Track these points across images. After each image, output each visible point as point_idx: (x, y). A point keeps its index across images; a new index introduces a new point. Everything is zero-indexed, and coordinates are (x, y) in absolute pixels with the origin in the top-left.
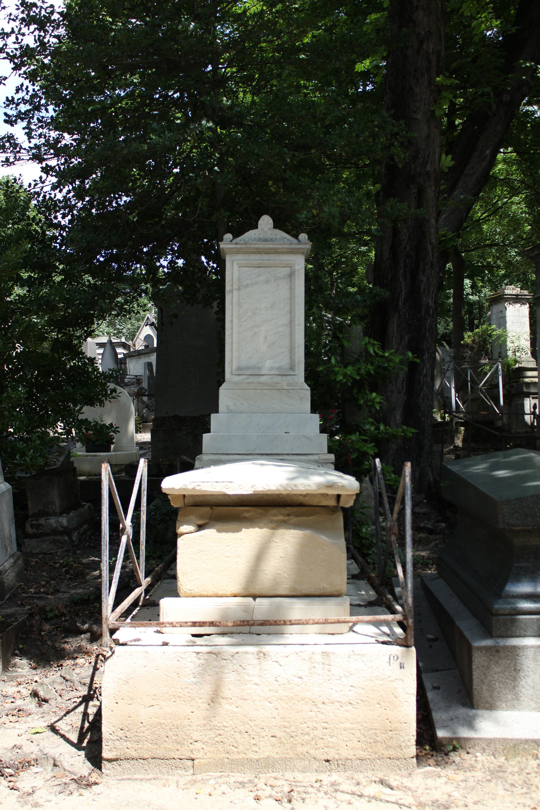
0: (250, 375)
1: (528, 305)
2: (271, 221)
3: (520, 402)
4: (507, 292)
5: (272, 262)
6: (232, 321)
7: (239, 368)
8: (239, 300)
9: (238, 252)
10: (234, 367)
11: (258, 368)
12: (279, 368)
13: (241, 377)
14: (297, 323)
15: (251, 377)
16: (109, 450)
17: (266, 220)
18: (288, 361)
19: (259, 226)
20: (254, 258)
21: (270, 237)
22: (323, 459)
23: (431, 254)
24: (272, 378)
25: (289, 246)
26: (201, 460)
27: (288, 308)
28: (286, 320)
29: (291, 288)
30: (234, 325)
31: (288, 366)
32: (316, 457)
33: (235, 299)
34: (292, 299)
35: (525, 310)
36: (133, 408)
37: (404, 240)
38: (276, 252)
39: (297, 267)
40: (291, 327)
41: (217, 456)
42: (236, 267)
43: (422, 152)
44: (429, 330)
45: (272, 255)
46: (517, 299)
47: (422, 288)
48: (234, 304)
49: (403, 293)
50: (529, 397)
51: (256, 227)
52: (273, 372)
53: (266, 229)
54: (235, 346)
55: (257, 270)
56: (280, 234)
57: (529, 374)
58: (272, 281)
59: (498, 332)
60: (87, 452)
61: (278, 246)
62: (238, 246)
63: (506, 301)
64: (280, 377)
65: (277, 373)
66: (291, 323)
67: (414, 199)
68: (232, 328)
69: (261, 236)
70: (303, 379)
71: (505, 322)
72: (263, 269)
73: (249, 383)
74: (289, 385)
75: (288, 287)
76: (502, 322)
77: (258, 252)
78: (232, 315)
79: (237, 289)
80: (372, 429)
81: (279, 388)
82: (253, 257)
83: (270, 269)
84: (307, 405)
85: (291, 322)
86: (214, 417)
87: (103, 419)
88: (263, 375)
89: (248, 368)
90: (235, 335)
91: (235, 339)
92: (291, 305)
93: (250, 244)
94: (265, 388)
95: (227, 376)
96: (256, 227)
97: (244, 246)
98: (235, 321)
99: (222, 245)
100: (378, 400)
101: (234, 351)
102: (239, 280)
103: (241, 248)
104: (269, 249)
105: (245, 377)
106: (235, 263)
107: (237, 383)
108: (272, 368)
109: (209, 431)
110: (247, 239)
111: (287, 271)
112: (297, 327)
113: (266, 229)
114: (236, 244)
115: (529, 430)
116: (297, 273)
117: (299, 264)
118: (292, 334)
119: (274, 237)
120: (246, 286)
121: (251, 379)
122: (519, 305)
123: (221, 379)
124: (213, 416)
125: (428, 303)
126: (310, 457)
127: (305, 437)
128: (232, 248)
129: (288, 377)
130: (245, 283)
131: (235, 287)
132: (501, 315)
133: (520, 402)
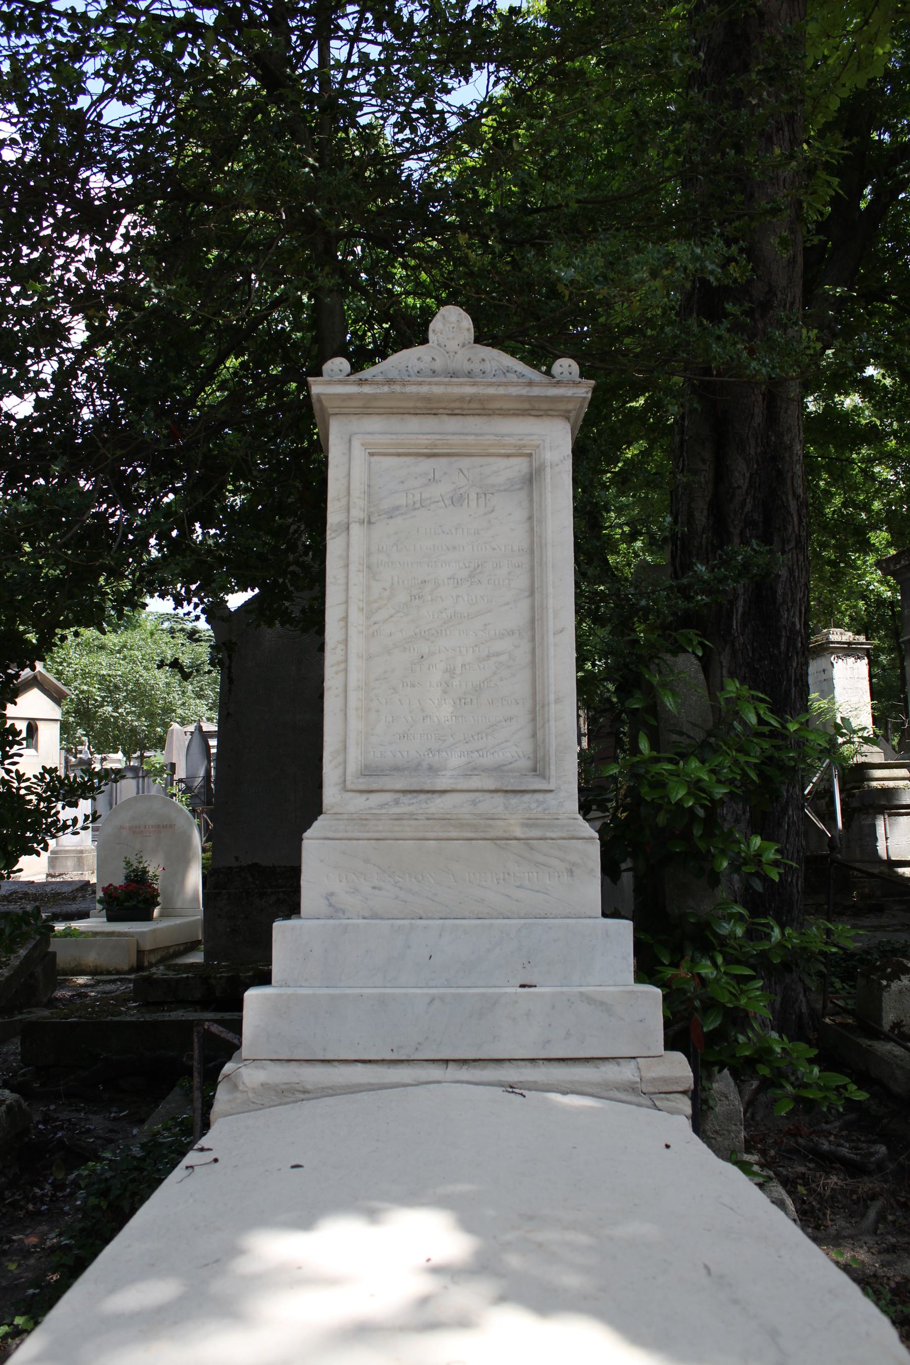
0: (404, 792)
1: (866, 661)
2: (467, 322)
3: (869, 822)
4: (833, 638)
5: (470, 438)
6: (346, 619)
7: (368, 771)
8: (369, 554)
9: (366, 408)
10: (352, 767)
11: (430, 768)
12: (498, 770)
13: (376, 799)
14: (551, 625)
15: (405, 799)
16: (148, 917)
17: (453, 318)
18: (526, 747)
19: (431, 336)
20: (419, 431)
21: (467, 366)
22: (653, 1080)
23: (795, 519)
24: (474, 803)
25: (524, 391)
26: (236, 1087)
27: (521, 581)
28: (517, 616)
29: (530, 518)
30: (353, 631)
31: (526, 764)
32: (627, 1073)
33: (356, 552)
34: (534, 549)
35: (862, 667)
36: (197, 840)
37: (739, 487)
38: (484, 408)
39: (549, 456)
40: (533, 639)
41: (293, 1068)
42: (358, 453)
43: (779, 294)
44: (796, 681)
45: (471, 420)
46: (849, 650)
47: (780, 591)
48: (353, 567)
49: (741, 603)
50: (883, 814)
51: (425, 341)
52: (475, 783)
53: (453, 345)
54: (354, 699)
55: (427, 465)
56: (497, 359)
57: (878, 773)
58: (473, 496)
59: (824, 704)
60: (110, 919)
61: (491, 391)
62: (367, 389)
63: (832, 653)
64: (499, 799)
65: (490, 784)
66: (534, 624)
67: (760, 398)
68: (346, 641)
69: (438, 365)
70: (573, 804)
71: (832, 688)
72: (443, 460)
73: (399, 818)
74: (529, 823)
75: (520, 514)
76: (828, 688)
77: (430, 408)
78: (347, 602)
79: (362, 522)
80: (739, 932)
81: (500, 834)
82: (414, 424)
83: (465, 463)
84: (591, 888)
85: (533, 621)
86: (283, 932)
87: (144, 859)
88: (444, 792)
89: (397, 769)
90: (354, 663)
91: (354, 678)
92: (532, 569)
93: (404, 384)
94: (454, 834)
95: (330, 794)
96: (425, 341)
97: (386, 389)
98: (355, 617)
99: (317, 387)
100: (771, 855)
101: (352, 713)
102: (369, 492)
103: (375, 397)
104: (461, 399)
105: (388, 797)
106: (356, 443)
107: (360, 819)
108: (472, 770)
109: (265, 979)
110: (393, 374)
111: (519, 466)
112: (551, 639)
113: (453, 345)
114: (361, 382)
115: (884, 869)
116: (548, 469)
117: (556, 443)
118: (536, 662)
119: (476, 366)
120: (391, 513)
121: (408, 805)
122: (853, 659)
123: (312, 807)
124: (280, 928)
125: (794, 624)
126: (610, 1072)
127: (589, 999)
128: (350, 397)
129: (527, 797)
130: (386, 505)
131: (356, 513)
132: (824, 677)
133: (869, 822)
